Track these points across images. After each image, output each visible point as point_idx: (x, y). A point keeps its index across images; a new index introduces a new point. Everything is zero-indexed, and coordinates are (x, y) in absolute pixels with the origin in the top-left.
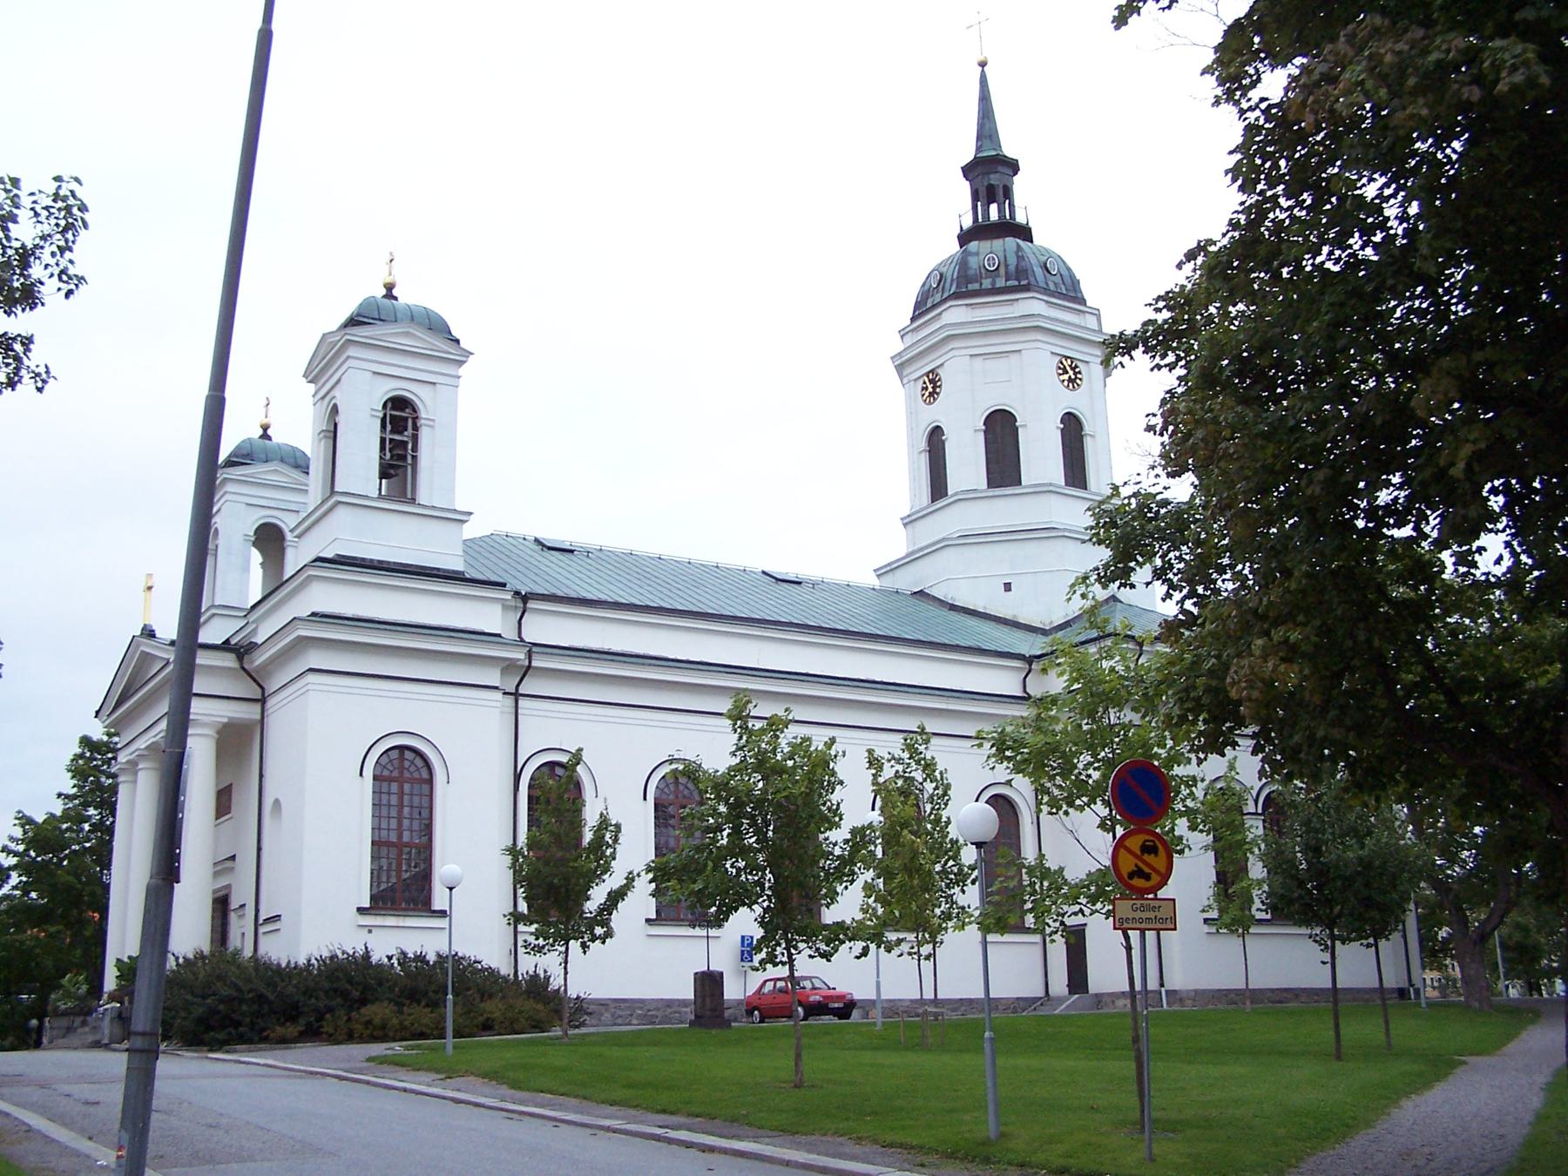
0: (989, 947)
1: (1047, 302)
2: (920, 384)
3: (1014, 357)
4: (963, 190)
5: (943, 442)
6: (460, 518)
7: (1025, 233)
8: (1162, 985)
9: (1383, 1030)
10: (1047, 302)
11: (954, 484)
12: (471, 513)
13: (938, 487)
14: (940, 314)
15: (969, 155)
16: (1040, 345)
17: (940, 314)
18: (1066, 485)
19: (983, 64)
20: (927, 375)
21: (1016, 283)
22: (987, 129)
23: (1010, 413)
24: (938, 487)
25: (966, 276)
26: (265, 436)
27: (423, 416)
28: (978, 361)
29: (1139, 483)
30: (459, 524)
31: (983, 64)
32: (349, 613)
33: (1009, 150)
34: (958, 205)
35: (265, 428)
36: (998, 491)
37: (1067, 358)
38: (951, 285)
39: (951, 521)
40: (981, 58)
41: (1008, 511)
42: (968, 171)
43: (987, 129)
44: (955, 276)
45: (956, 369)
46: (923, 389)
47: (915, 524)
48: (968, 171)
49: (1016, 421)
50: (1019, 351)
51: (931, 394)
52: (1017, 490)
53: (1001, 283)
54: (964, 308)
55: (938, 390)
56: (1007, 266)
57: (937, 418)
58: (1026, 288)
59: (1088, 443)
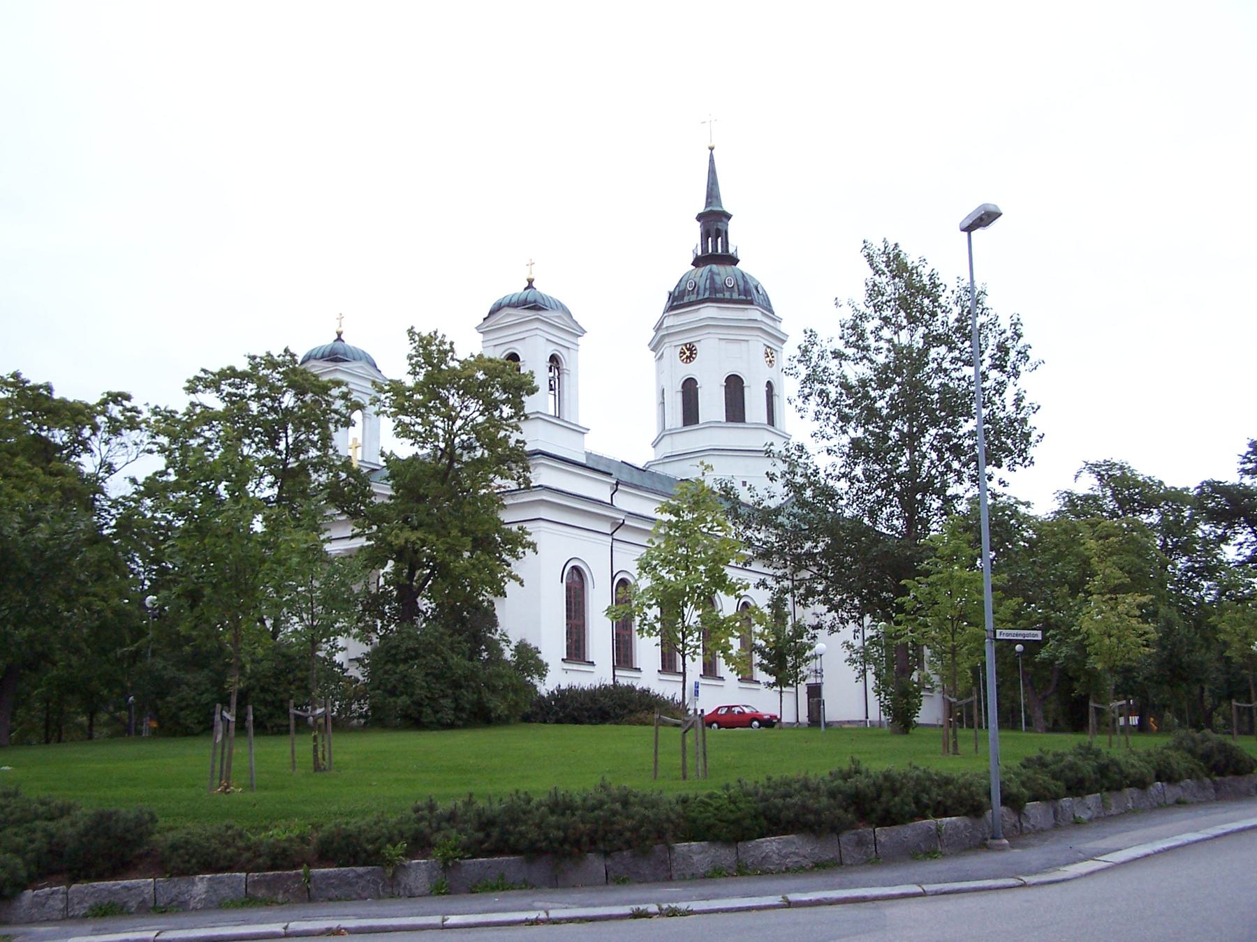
0: (783, 694)
1: (762, 313)
2: (679, 349)
3: (744, 344)
4: (696, 229)
5: (697, 390)
6: (582, 431)
7: (734, 261)
8: (867, 718)
9: (659, 763)
10: (762, 313)
11: (703, 416)
12: (589, 430)
13: (691, 415)
14: (699, 309)
15: (701, 208)
16: (760, 339)
17: (699, 309)
18: (728, 419)
19: (712, 149)
20: (686, 345)
21: (744, 298)
22: (713, 193)
23: (741, 379)
24: (691, 415)
25: (715, 288)
26: (339, 339)
27: (564, 367)
28: (723, 343)
29: (735, 410)
30: (580, 435)
31: (712, 149)
32: (554, 486)
33: (727, 206)
34: (691, 238)
35: (339, 334)
36: (730, 424)
37: (769, 347)
38: (705, 292)
39: (695, 439)
40: (711, 145)
41: (734, 437)
42: (700, 217)
43: (713, 193)
44: (708, 286)
45: (708, 347)
46: (681, 353)
47: (673, 436)
48: (700, 217)
49: (743, 383)
50: (748, 341)
51: (687, 357)
52: (740, 425)
53: (735, 296)
54: (715, 309)
55: (694, 356)
56: (738, 286)
57: (694, 373)
58: (751, 303)
59: (746, 390)
